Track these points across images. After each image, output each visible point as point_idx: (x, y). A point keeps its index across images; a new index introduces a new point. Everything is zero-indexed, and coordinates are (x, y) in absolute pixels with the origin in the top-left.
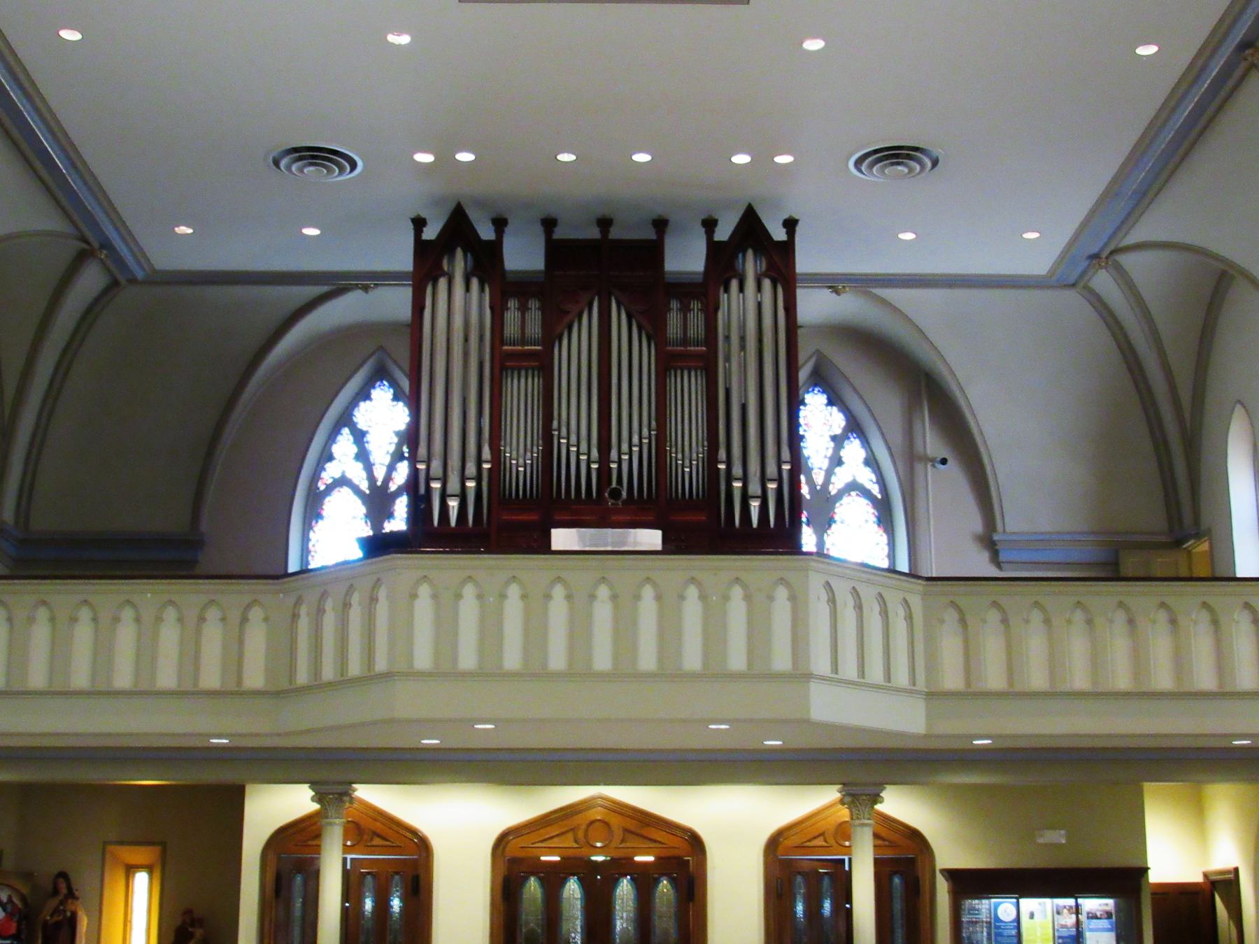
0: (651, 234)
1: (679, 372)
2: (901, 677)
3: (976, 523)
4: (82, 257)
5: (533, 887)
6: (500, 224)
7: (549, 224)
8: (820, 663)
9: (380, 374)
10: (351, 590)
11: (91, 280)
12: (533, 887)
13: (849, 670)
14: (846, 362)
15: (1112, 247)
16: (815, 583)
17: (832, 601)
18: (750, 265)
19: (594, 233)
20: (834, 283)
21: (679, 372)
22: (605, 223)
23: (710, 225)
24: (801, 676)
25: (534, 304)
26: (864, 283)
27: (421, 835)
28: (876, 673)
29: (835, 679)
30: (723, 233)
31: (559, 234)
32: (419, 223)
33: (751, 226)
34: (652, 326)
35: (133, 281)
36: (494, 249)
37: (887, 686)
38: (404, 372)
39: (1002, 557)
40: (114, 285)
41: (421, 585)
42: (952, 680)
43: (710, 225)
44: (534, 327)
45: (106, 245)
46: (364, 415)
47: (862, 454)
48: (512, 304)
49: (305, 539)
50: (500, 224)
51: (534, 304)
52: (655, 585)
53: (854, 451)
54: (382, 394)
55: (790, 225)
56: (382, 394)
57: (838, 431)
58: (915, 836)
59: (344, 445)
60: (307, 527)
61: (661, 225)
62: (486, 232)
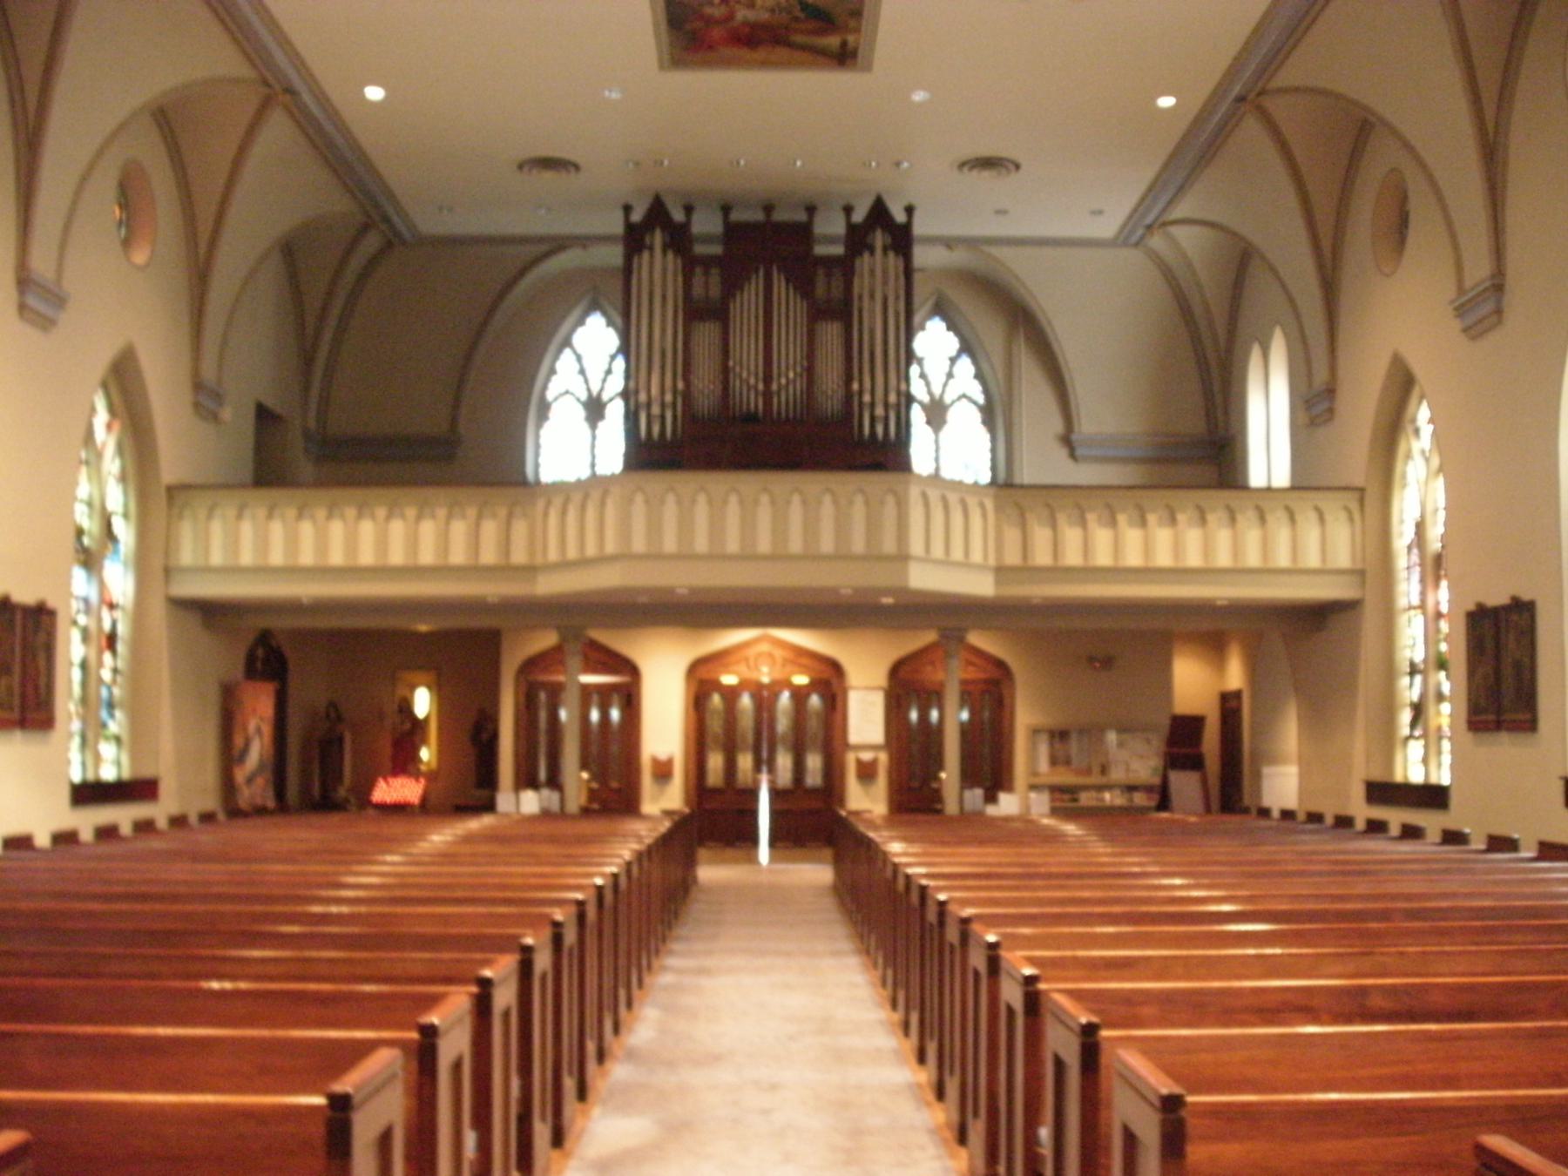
0: (802, 217)
1: (791, 415)
2: (977, 556)
3: (1058, 425)
4: (365, 228)
5: (716, 699)
6: (689, 210)
7: (726, 210)
8: (916, 546)
9: (594, 306)
10: (586, 497)
11: (372, 243)
12: (716, 699)
13: (938, 551)
14: (960, 298)
15: (1161, 220)
16: (914, 492)
17: (927, 504)
18: (879, 239)
19: (759, 216)
20: (949, 243)
21: (791, 415)
22: (768, 209)
23: (848, 210)
24: (903, 557)
25: (715, 271)
26: (972, 243)
27: (1225, 603)
28: (957, 554)
29: (927, 559)
30: (859, 216)
31: (736, 216)
32: (627, 209)
33: (879, 211)
34: (804, 287)
35: (404, 243)
36: (685, 227)
37: (966, 565)
38: (616, 309)
39: (1079, 452)
40: (388, 246)
41: (581, 322)
42: (1013, 558)
43: (848, 210)
44: (715, 291)
45: (290, 91)
46: (581, 337)
47: (971, 370)
48: (698, 271)
49: (537, 436)
50: (689, 210)
51: (715, 271)
52: (801, 493)
53: (966, 366)
54: (596, 321)
55: (910, 210)
56: (596, 321)
57: (953, 353)
58: (1000, 665)
59: (566, 362)
60: (539, 426)
61: (811, 210)
62: (678, 216)
